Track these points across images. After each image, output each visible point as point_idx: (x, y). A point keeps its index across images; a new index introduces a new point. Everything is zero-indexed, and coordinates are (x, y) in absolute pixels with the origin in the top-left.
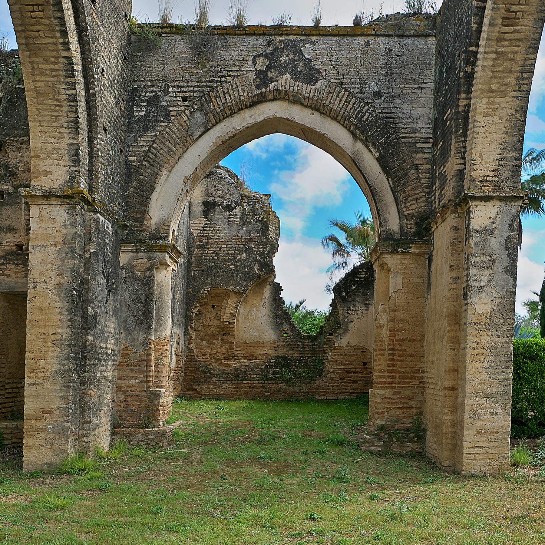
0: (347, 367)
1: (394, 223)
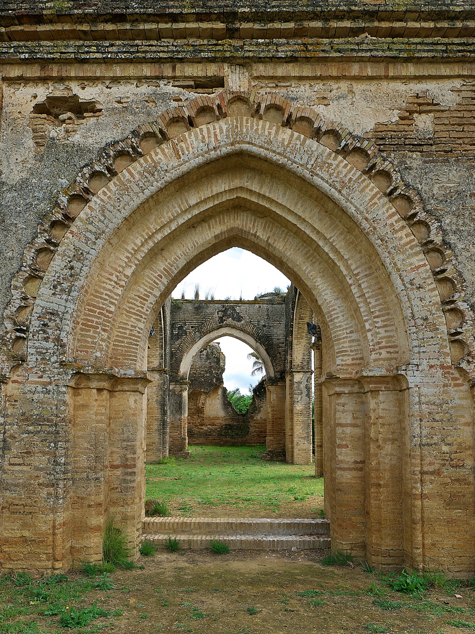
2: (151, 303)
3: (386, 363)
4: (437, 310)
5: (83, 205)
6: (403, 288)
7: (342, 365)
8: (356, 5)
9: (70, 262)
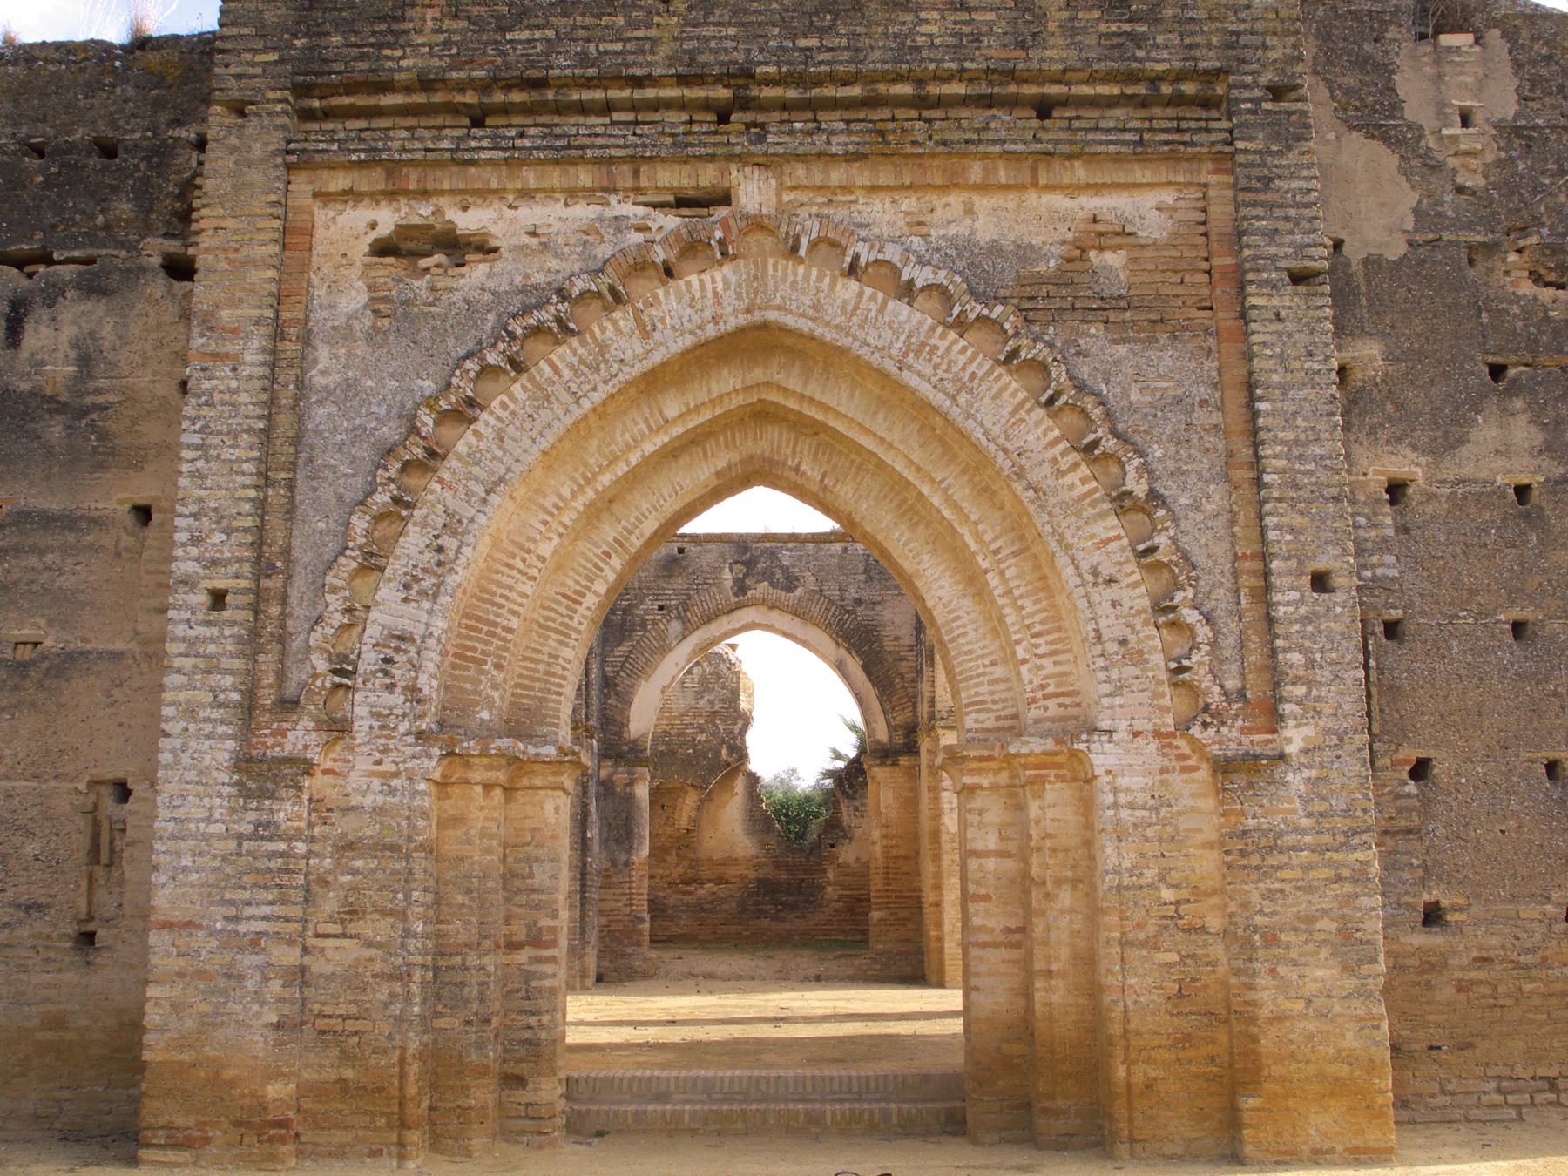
1: (882, 735)
2: (589, 608)
4: (1146, 623)
6: (1079, 581)
7: (977, 731)
8: (972, 60)
9: (437, 537)
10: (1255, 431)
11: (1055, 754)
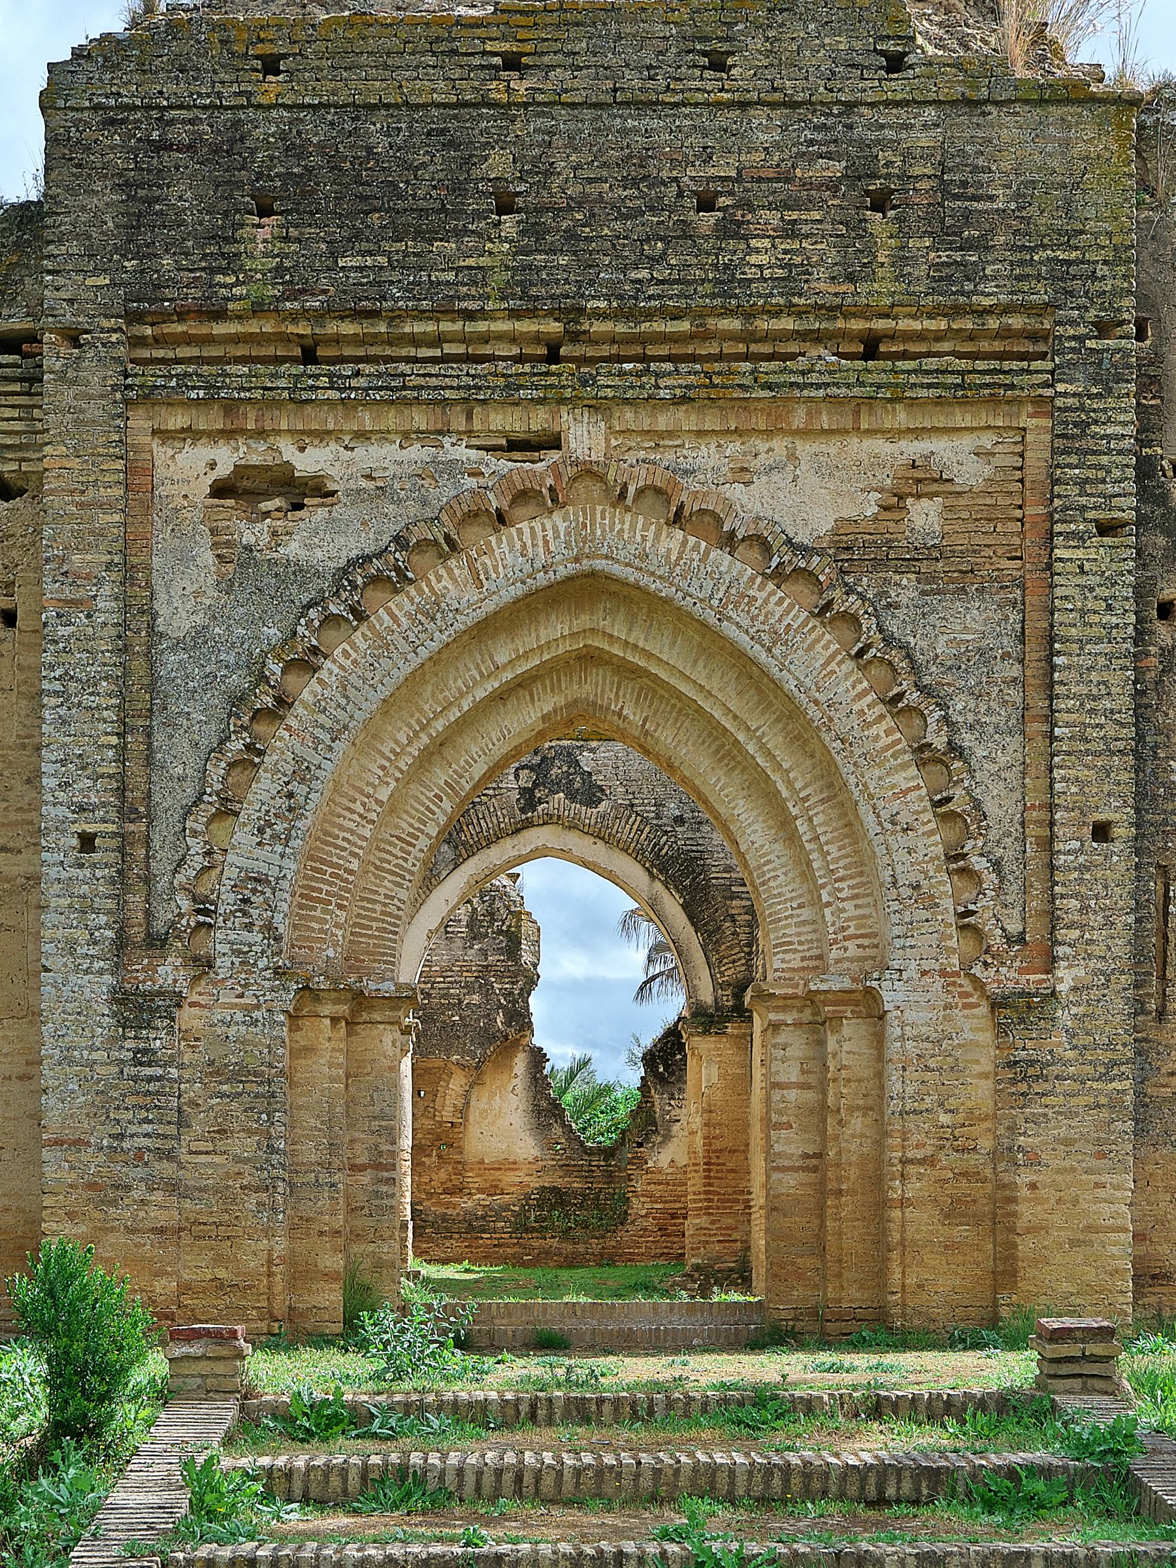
0: (672, 1205)
2: (421, 851)
3: (855, 967)
5: (307, 677)
6: (878, 829)
7: (783, 970)
8: (800, 295)
9: (287, 783)
10: (1051, 684)
11: (851, 992)
